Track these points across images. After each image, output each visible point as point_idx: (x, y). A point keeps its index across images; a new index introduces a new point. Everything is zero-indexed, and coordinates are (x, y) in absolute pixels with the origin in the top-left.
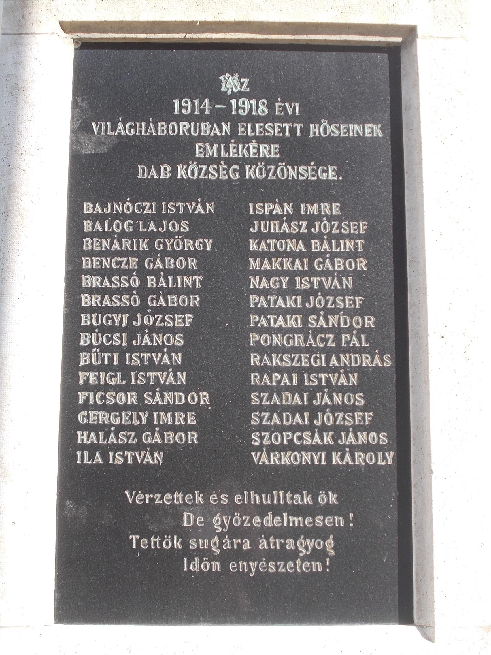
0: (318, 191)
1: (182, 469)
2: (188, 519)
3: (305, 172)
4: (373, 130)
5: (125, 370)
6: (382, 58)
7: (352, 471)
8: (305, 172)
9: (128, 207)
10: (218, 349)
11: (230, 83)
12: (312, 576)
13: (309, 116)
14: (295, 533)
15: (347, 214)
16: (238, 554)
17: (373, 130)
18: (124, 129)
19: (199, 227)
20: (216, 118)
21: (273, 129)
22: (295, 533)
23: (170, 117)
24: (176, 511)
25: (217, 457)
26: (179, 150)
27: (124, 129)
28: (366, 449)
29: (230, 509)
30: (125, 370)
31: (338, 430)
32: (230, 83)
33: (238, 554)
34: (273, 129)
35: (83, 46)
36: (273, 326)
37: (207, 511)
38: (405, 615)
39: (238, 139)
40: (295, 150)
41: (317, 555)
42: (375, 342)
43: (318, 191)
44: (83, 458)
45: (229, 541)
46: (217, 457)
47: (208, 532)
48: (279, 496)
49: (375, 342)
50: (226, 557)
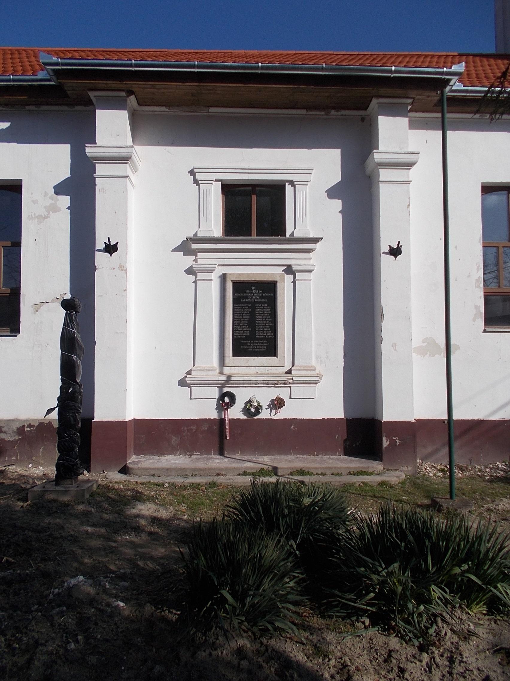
0: (264, 303)
1: (247, 338)
2: (248, 344)
3: (263, 300)
4: (272, 295)
5: (240, 326)
6: (495, 248)
7: (268, 338)
8: (263, 300)
9: (240, 305)
10: (252, 323)
11: (253, 288)
12: (263, 351)
13: (263, 293)
14: (261, 346)
15: (268, 306)
16: (254, 348)
17: (272, 295)
18: (239, 295)
19: (249, 307)
20: (251, 293)
21: (258, 295)
22: (261, 346)
23: (245, 293)
24: (247, 343)
25: (252, 337)
26: (247, 297)
27: (239, 295)
28: (270, 335)
29: (253, 343)
30: (240, 326)
31: (267, 333)
32: (253, 288)
33: (254, 348)
34: (258, 295)
35: (233, 283)
36: (259, 320)
37: (251, 343)
38: (275, 356)
39: (255, 296)
40: (261, 297)
41: (264, 348)
42: (271, 322)
43: (264, 303)
44: (235, 337)
45: (475, 621)
46: (252, 337)
47: (251, 346)
48: (260, 341)
49: (271, 322)
50: (253, 349)
